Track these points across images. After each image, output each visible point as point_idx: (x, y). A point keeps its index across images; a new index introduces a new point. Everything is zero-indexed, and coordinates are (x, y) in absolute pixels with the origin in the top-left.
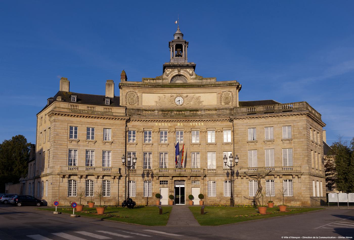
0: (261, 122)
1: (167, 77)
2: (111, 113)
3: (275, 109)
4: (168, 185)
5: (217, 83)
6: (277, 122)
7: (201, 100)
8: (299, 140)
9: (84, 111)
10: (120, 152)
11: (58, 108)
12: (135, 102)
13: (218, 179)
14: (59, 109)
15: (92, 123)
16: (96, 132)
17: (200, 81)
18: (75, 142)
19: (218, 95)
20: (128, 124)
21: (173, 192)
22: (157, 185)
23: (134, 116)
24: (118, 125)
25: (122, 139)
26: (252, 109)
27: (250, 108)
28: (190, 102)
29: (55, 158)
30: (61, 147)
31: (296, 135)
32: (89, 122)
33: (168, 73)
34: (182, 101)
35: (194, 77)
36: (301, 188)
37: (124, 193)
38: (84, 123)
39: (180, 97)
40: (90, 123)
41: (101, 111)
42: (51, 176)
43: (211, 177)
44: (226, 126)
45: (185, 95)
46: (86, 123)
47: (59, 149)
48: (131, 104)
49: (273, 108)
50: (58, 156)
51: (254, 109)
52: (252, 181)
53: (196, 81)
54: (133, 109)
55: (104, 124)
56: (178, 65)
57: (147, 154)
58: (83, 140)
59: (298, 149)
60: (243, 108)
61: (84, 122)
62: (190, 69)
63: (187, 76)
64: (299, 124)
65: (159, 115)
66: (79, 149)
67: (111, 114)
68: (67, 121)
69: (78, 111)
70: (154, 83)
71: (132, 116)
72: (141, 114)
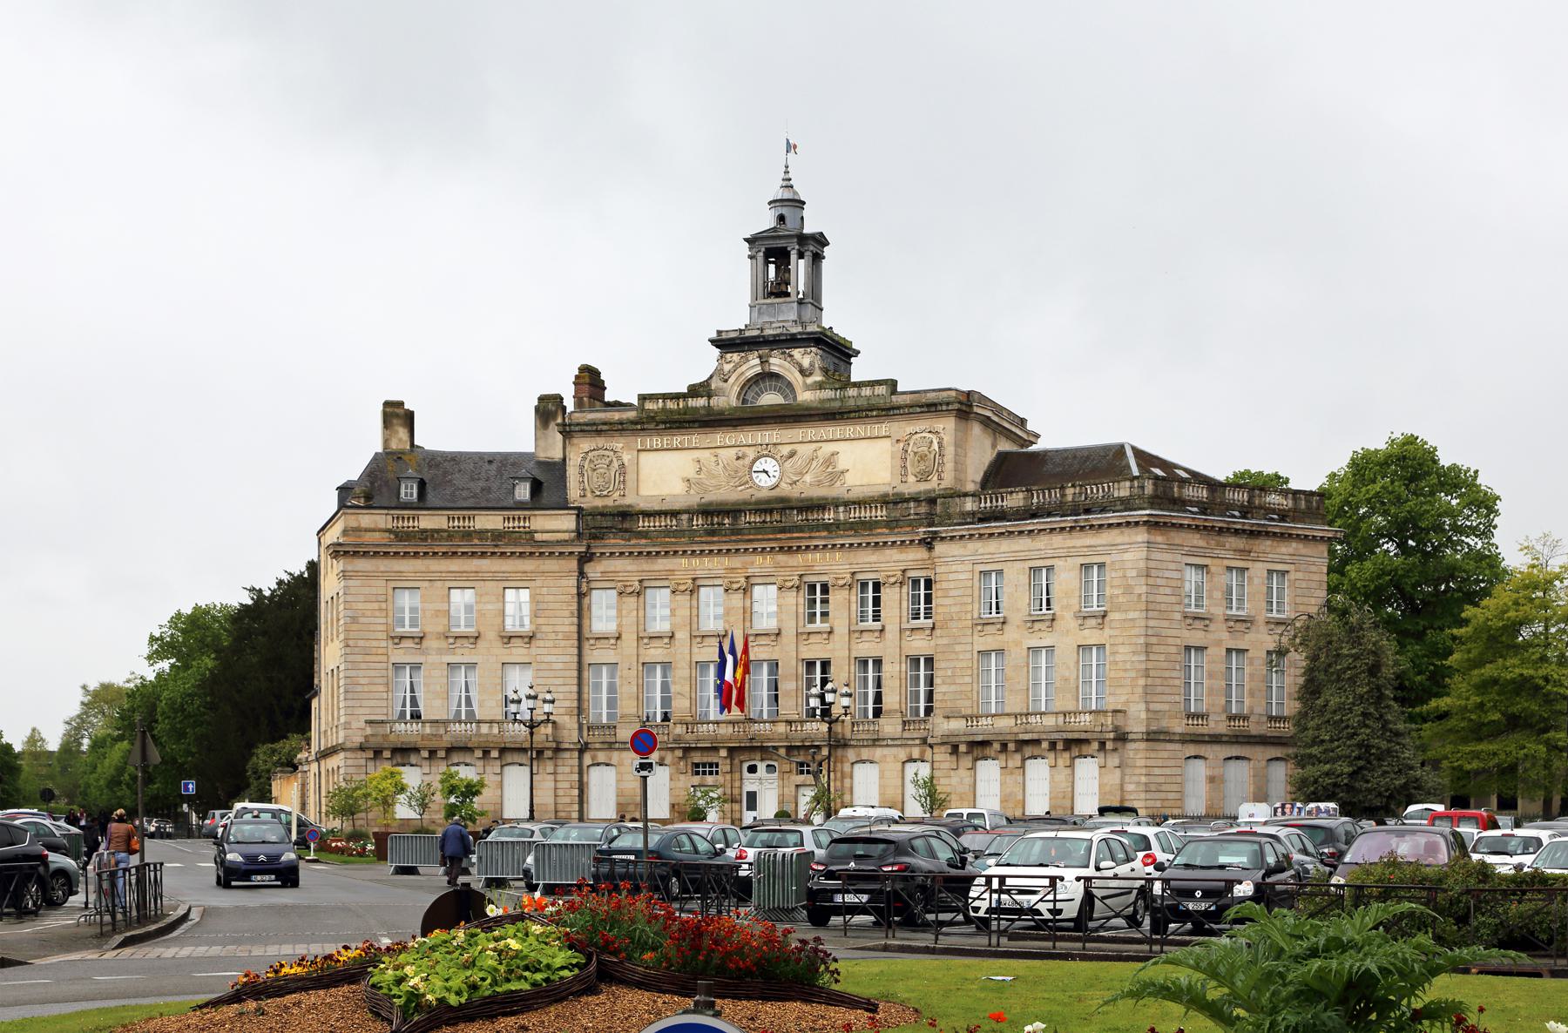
1: (725, 385)
2: (526, 533)
7: (840, 467)
10: (560, 666)
12: (611, 489)
13: (885, 756)
16: (480, 602)
19: (897, 445)
20: (588, 568)
21: (736, 802)
22: (682, 777)
23: (609, 538)
25: (567, 621)
28: (802, 474)
30: (368, 658)
35: (818, 377)
37: (576, 807)
39: (769, 459)
42: (342, 755)
43: (863, 750)
45: (785, 450)
47: (363, 666)
48: (598, 493)
50: (359, 688)
57: (814, 663)
58: (438, 633)
59: (1121, 649)
63: (794, 376)
64: (1127, 556)
70: (678, 412)
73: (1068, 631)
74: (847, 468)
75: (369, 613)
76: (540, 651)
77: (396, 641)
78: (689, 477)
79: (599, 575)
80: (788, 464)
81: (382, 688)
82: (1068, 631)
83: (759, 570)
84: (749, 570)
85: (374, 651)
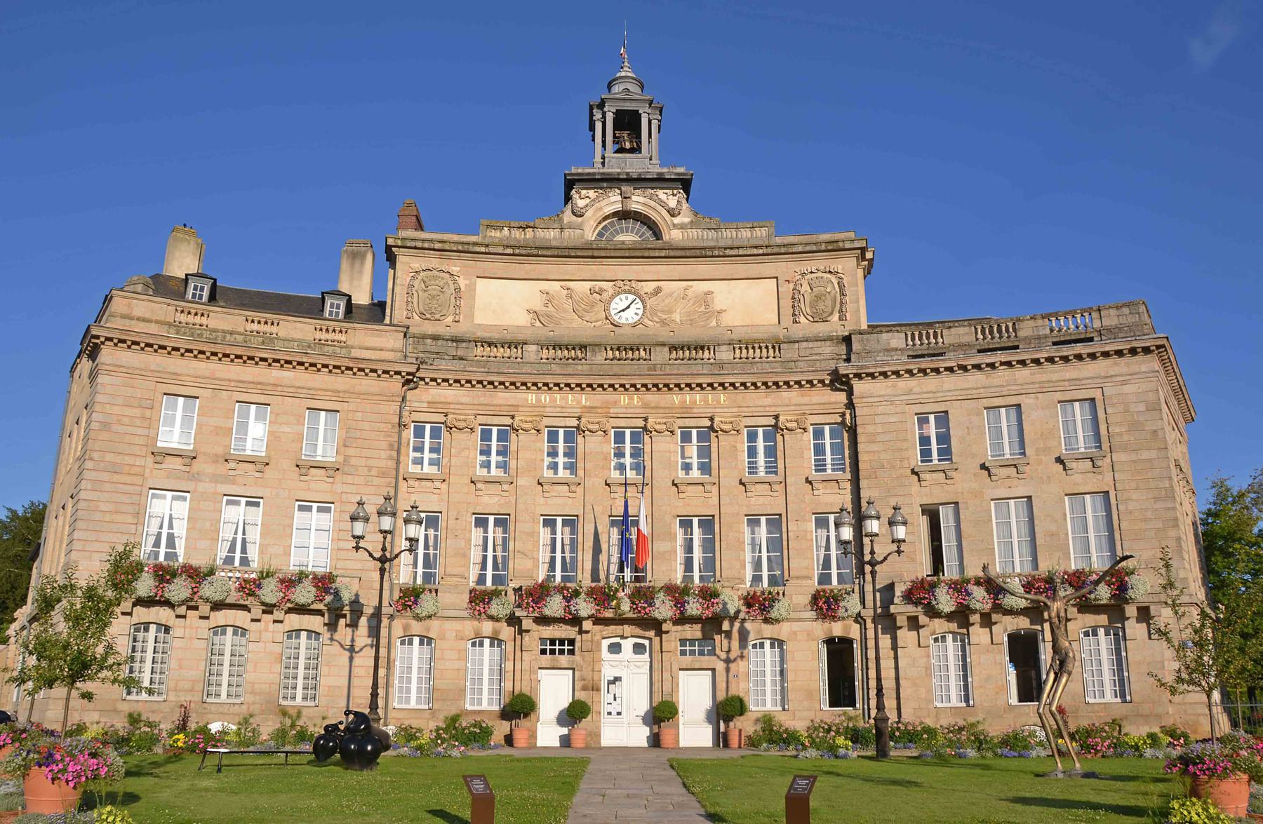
0: (966, 386)
2: (341, 347)
3: (1021, 334)
4: (577, 657)
5: (779, 240)
6: (1037, 386)
8: (1133, 457)
9: (228, 337)
11: (123, 317)
13: (795, 633)
14: (127, 322)
15: (259, 387)
17: (712, 234)
18: (179, 459)
24: (370, 397)
25: (384, 454)
26: (928, 338)
27: (917, 333)
29: (84, 527)
30: (116, 478)
31: (1121, 435)
32: (245, 379)
33: (581, 203)
34: (638, 311)
36: (1162, 662)
38: (227, 383)
40: (249, 382)
41: (301, 337)
44: (822, 407)
46: (232, 384)
47: (108, 487)
49: (1011, 330)
50: (98, 516)
51: (935, 337)
52: (944, 638)
53: (693, 233)
54: (435, 338)
55: (311, 392)
56: (625, 177)
58: (216, 455)
59: (1135, 496)
60: (890, 334)
61: (224, 380)
62: (670, 192)
64: (1128, 389)
65: (544, 363)
66: (195, 491)
67: (344, 351)
68: (152, 371)
69: (206, 334)
71: (431, 365)
72: (470, 356)
73: (1049, 477)
74: (724, 308)
75: (126, 420)
76: (346, 488)
77: (159, 458)
78: (535, 309)
79: (425, 405)
80: (651, 302)
81: (130, 519)
82: (1049, 477)
83: (624, 410)
84: (612, 411)
85: (126, 469)
